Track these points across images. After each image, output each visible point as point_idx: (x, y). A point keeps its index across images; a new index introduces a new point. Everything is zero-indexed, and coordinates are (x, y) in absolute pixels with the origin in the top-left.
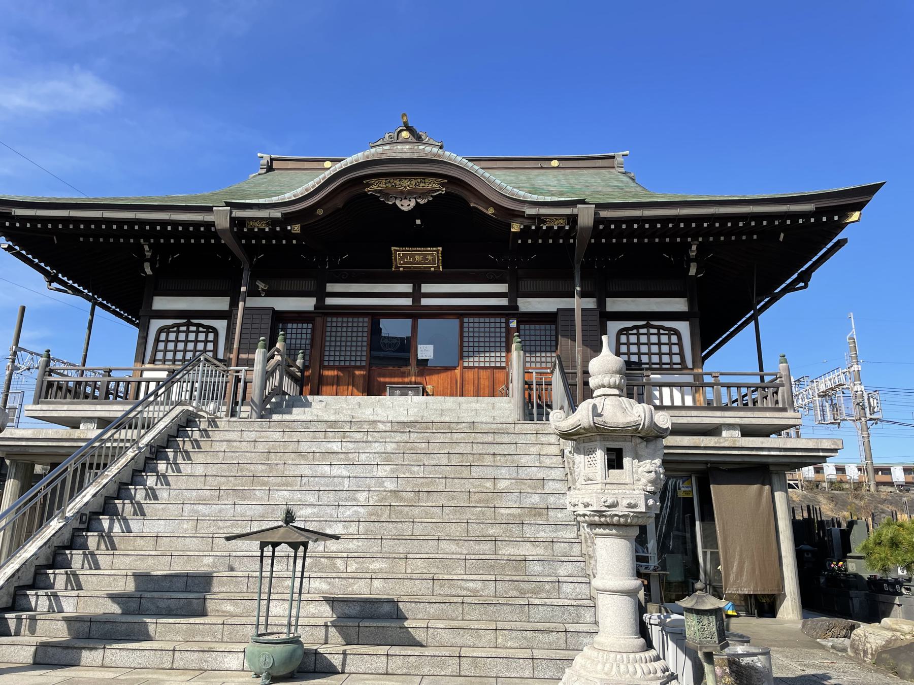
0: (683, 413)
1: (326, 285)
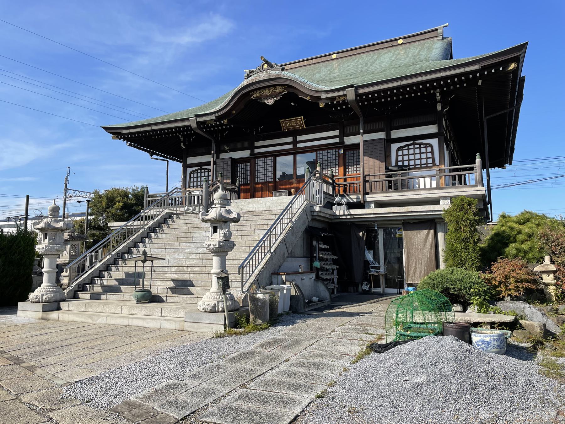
1: (478, 81)
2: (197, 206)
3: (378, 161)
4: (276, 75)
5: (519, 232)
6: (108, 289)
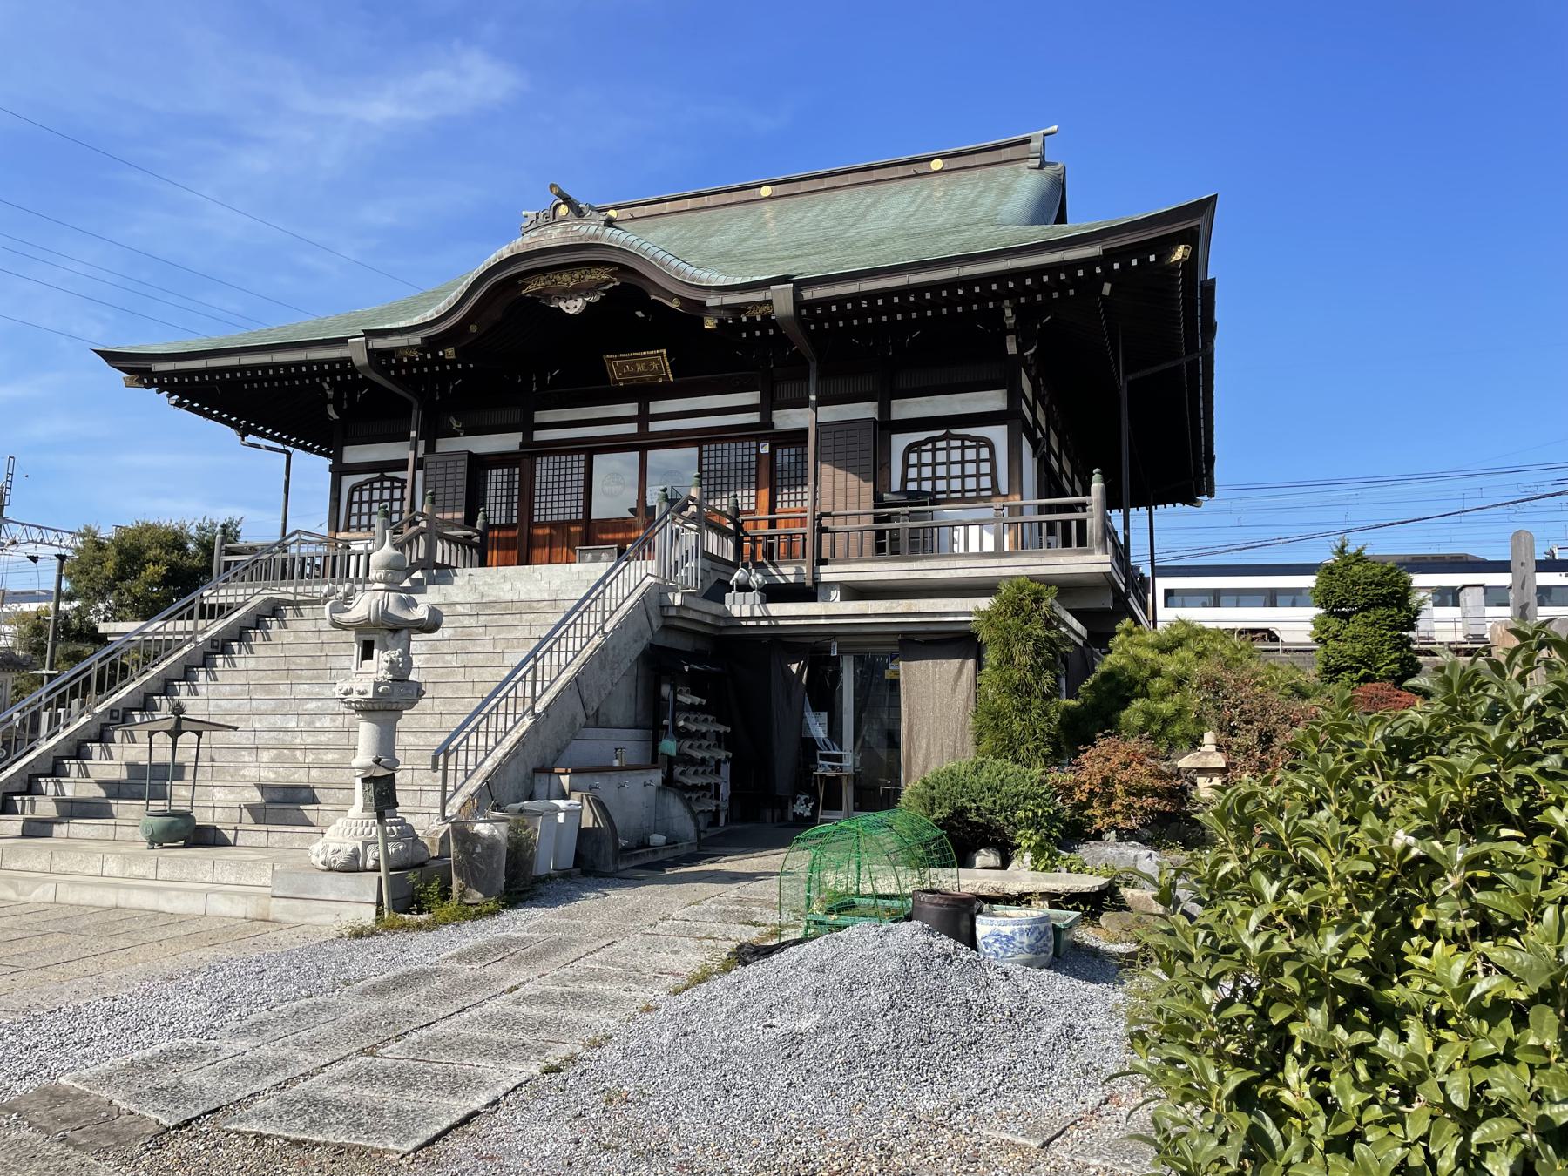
0: (981, 563)
2: (359, 582)
3: (856, 478)
4: (590, 237)
5: (1156, 673)
6: (74, 810)
